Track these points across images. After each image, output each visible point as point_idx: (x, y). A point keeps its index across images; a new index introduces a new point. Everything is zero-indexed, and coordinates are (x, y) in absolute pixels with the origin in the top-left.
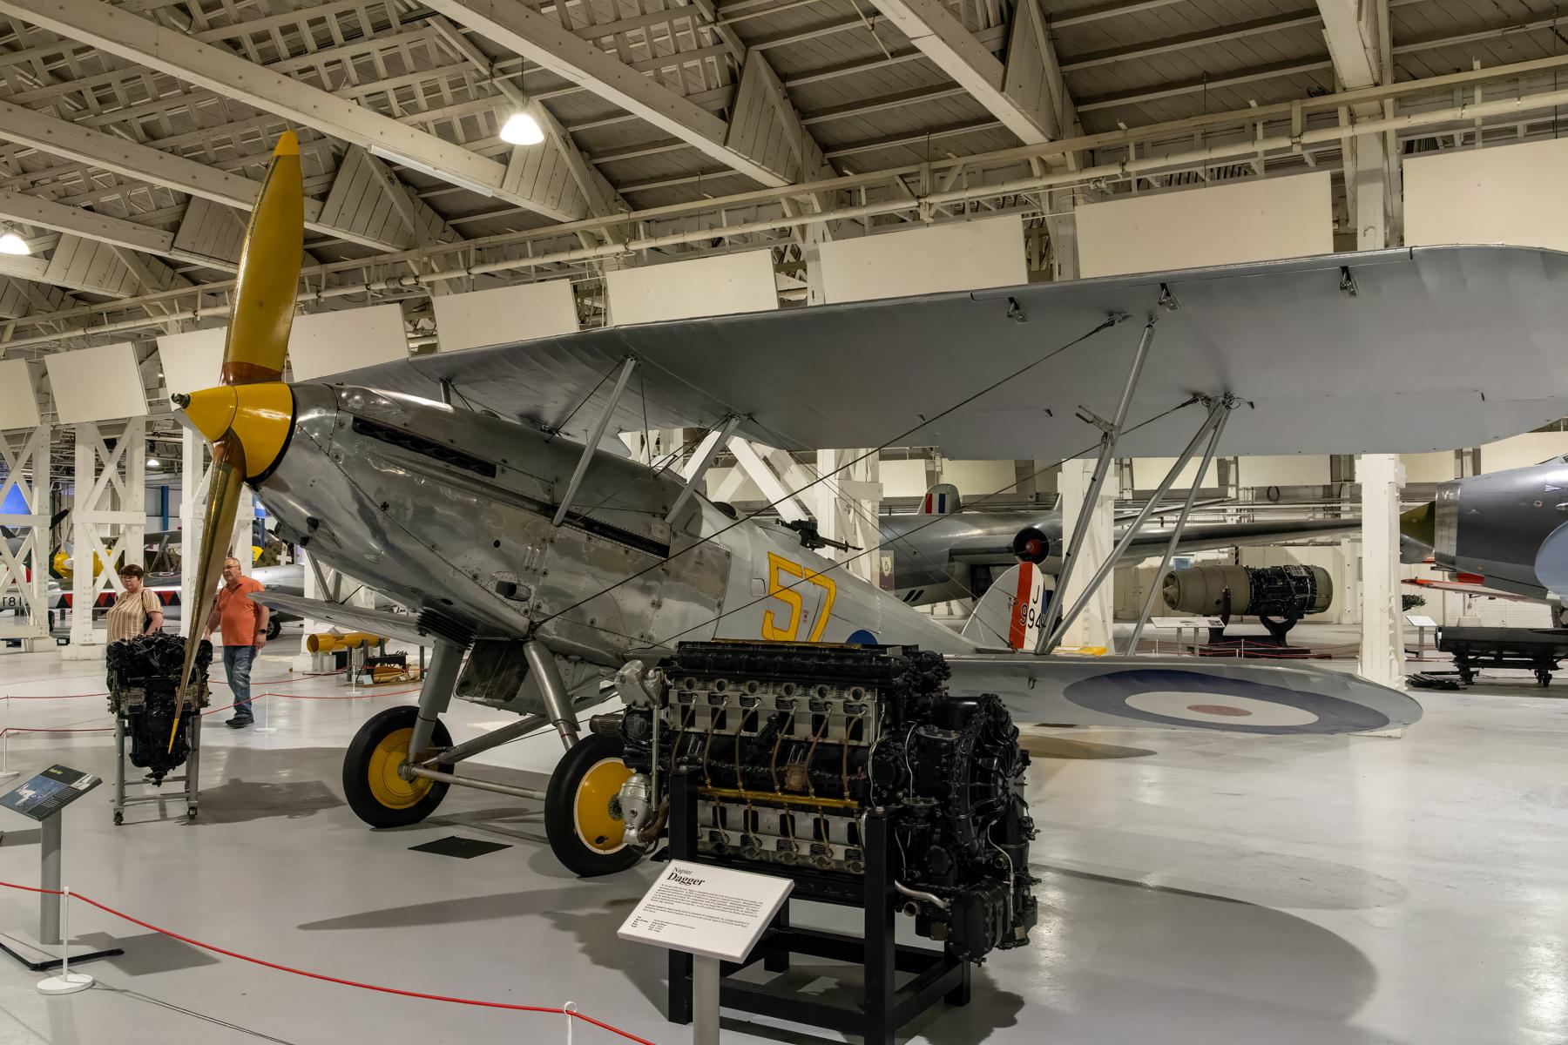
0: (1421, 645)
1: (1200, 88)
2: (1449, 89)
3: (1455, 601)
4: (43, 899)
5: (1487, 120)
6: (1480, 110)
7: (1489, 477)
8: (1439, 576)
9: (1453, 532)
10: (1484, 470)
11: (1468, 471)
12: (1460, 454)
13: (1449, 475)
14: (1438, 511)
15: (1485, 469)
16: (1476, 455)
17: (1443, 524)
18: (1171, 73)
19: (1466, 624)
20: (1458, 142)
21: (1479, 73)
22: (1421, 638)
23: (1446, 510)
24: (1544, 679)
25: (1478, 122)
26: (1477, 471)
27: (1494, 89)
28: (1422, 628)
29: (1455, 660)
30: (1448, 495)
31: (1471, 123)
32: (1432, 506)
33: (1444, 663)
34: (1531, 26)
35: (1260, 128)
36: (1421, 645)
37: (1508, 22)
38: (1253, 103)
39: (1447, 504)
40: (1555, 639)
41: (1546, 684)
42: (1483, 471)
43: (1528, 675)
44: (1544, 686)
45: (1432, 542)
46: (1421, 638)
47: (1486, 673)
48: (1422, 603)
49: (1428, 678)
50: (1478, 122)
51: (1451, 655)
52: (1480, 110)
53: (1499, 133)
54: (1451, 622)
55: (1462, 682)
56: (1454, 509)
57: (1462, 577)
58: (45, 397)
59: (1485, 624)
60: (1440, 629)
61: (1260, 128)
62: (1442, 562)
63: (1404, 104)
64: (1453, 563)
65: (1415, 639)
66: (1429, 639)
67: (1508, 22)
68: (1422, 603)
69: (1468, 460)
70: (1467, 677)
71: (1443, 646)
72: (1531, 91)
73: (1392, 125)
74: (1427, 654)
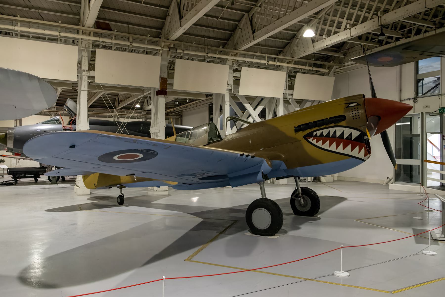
0: (3, 174)
1: (127, 25)
2: (12, 20)
3: (14, 161)
4: (415, 238)
5: (21, 31)
6: (19, 28)
7: (23, 126)
8: (9, 154)
9: (12, 142)
10: (23, 125)
11: (18, 125)
12: (16, 120)
13: (13, 126)
14: (8, 136)
15: (23, 124)
16: (20, 121)
17: (9, 139)
18: (132, 21)
19: (17, 167)
20: (113, 49)
21: (18, 18)
22: (4, 172)
23: (10, 136)
24: (36, 180)
25: (19, 31)
26: (21, 125)
27: (23, 24)
28: (4, 169)
29: (13, 177)
30: (11, 131)
31: (17, 31)
32: (6, 134)
33: (10, 178)
34: (33, 10)
35: (146, 41)
36: (3, 174)
37: (27, 7)
38: (19, 16)
39: (11, 134)
40: (39, 170)
41: (37, 182)
42: (22, 125)
43: (32, 180)
44: (36, 182)
45: (6, 144)
46: (4, 172)
47: (22, 180)
48: (4, 162)
49: (5, 182)
50: (19, 31)
51: (12, 176)
52: (19, 28)
53: (25, 36)
54: (13, 167)
55: (15, 183)
56: (13, 135)
57: (16, 154)
58: (291, 87)
59: (22, 167)
60: (9, 169)
61: (146, 41)
62: (9, 150)
63: (95, 34)
64: (12, 150)
65: (2, 172)
66: (6, 172)
67: (27, 7)
68: (4, 162)
69: (18, 121)
70: (16, 181)
71: (9, 173)
72: (49, 29)
73: (92, 38)
74: (5, 176)
